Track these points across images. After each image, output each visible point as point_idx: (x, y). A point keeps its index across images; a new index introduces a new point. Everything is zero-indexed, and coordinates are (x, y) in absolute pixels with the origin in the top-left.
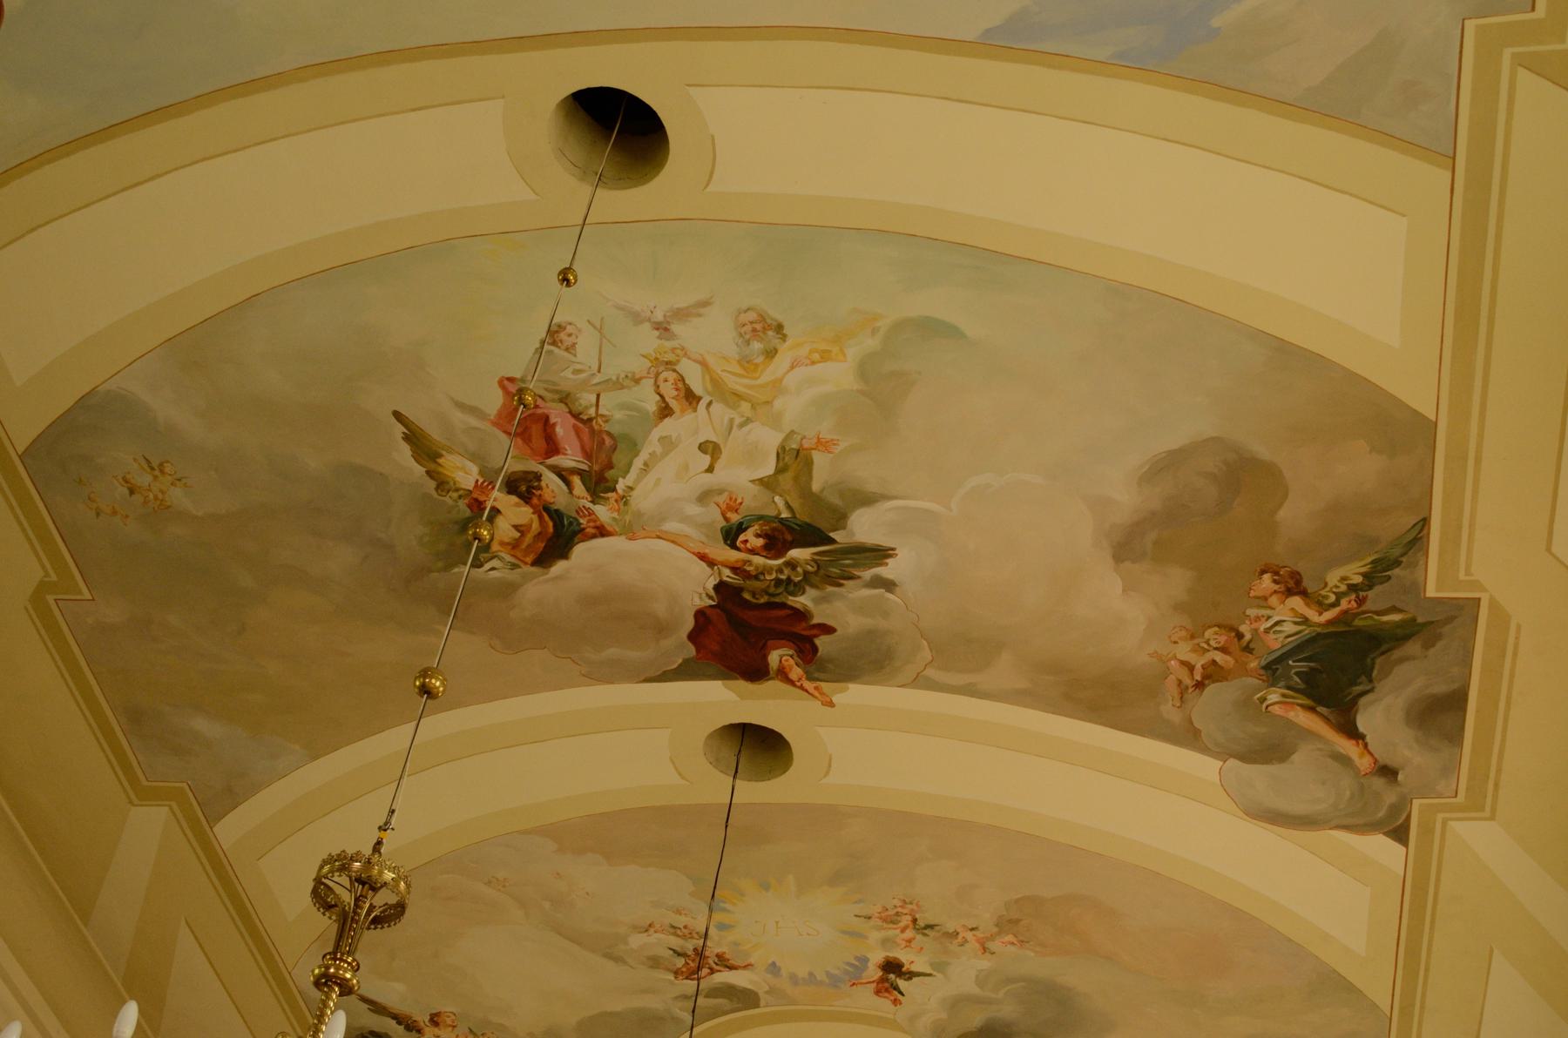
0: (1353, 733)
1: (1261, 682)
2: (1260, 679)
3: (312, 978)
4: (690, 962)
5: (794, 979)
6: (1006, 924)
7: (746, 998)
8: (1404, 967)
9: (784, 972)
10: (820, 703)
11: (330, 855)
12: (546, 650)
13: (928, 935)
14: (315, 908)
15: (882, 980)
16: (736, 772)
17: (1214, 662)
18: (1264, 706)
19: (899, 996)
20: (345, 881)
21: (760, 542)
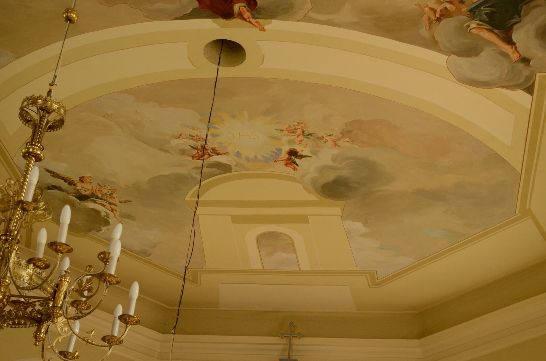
0: (509, 42)
1: (468, 18)
2: (467, 17)
3: (22, 154)
4: (199, 152)
5: (248, 159)
6: (346, 133)
7: (226, 168)
8: (528, 151)
9: (243, 156)
10: (258, 29)
11: (27, 97)
12: (126, 4)
13: (309, 139)
14: (21, 122)
15: (289, 159)
16: (219, 63)
17: (446, 8)
18: (469, 29)
19: (296, 167)
20: (35, 109)
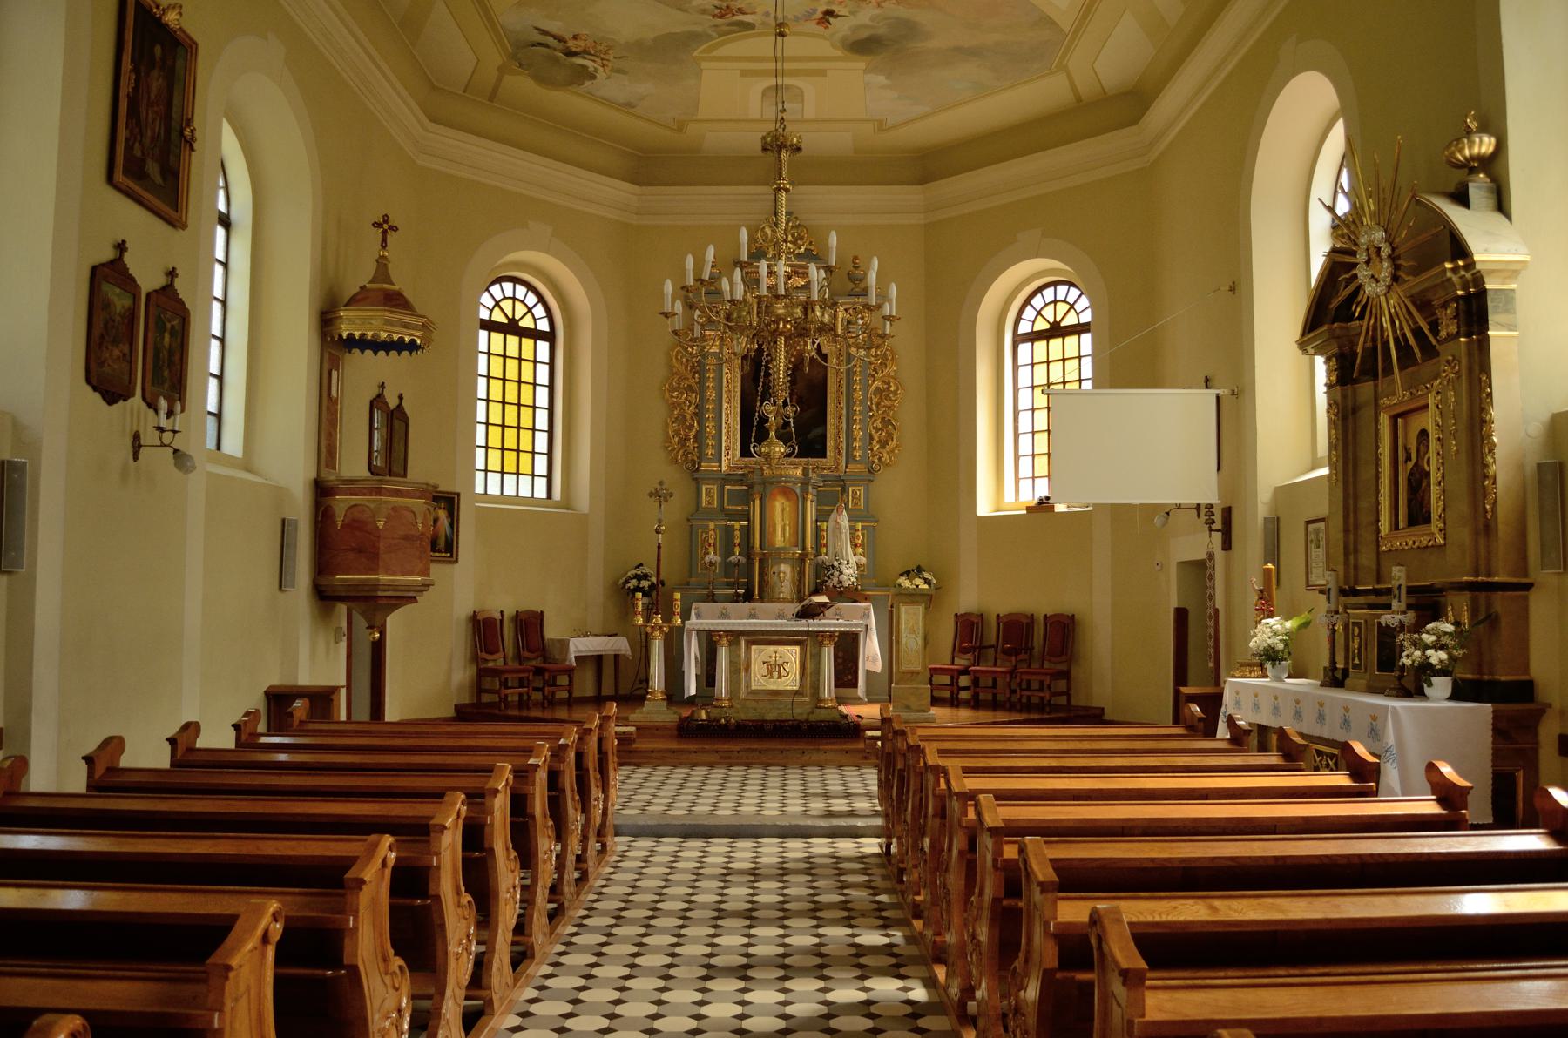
7: (749, 26)
21: (1411, 615)
